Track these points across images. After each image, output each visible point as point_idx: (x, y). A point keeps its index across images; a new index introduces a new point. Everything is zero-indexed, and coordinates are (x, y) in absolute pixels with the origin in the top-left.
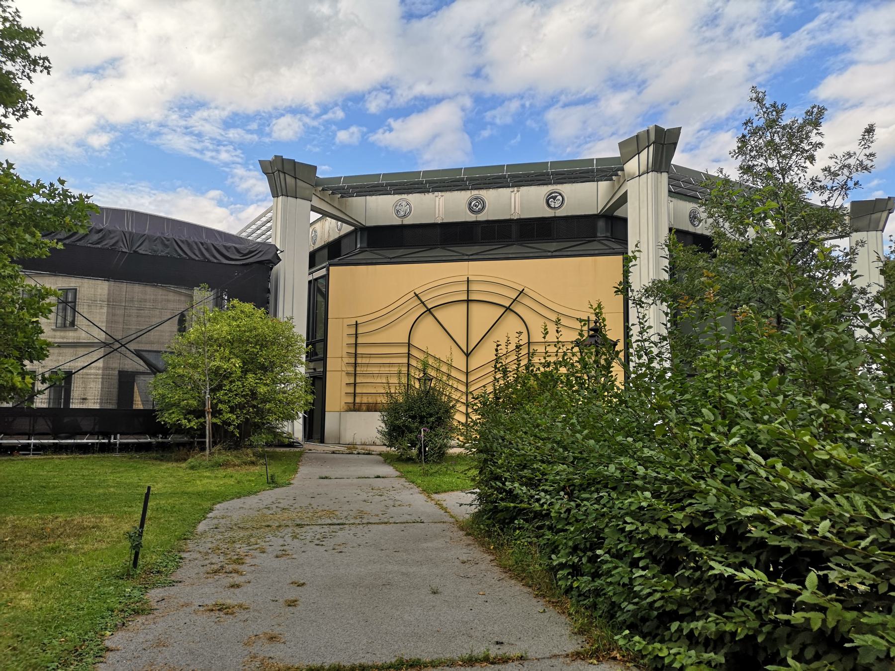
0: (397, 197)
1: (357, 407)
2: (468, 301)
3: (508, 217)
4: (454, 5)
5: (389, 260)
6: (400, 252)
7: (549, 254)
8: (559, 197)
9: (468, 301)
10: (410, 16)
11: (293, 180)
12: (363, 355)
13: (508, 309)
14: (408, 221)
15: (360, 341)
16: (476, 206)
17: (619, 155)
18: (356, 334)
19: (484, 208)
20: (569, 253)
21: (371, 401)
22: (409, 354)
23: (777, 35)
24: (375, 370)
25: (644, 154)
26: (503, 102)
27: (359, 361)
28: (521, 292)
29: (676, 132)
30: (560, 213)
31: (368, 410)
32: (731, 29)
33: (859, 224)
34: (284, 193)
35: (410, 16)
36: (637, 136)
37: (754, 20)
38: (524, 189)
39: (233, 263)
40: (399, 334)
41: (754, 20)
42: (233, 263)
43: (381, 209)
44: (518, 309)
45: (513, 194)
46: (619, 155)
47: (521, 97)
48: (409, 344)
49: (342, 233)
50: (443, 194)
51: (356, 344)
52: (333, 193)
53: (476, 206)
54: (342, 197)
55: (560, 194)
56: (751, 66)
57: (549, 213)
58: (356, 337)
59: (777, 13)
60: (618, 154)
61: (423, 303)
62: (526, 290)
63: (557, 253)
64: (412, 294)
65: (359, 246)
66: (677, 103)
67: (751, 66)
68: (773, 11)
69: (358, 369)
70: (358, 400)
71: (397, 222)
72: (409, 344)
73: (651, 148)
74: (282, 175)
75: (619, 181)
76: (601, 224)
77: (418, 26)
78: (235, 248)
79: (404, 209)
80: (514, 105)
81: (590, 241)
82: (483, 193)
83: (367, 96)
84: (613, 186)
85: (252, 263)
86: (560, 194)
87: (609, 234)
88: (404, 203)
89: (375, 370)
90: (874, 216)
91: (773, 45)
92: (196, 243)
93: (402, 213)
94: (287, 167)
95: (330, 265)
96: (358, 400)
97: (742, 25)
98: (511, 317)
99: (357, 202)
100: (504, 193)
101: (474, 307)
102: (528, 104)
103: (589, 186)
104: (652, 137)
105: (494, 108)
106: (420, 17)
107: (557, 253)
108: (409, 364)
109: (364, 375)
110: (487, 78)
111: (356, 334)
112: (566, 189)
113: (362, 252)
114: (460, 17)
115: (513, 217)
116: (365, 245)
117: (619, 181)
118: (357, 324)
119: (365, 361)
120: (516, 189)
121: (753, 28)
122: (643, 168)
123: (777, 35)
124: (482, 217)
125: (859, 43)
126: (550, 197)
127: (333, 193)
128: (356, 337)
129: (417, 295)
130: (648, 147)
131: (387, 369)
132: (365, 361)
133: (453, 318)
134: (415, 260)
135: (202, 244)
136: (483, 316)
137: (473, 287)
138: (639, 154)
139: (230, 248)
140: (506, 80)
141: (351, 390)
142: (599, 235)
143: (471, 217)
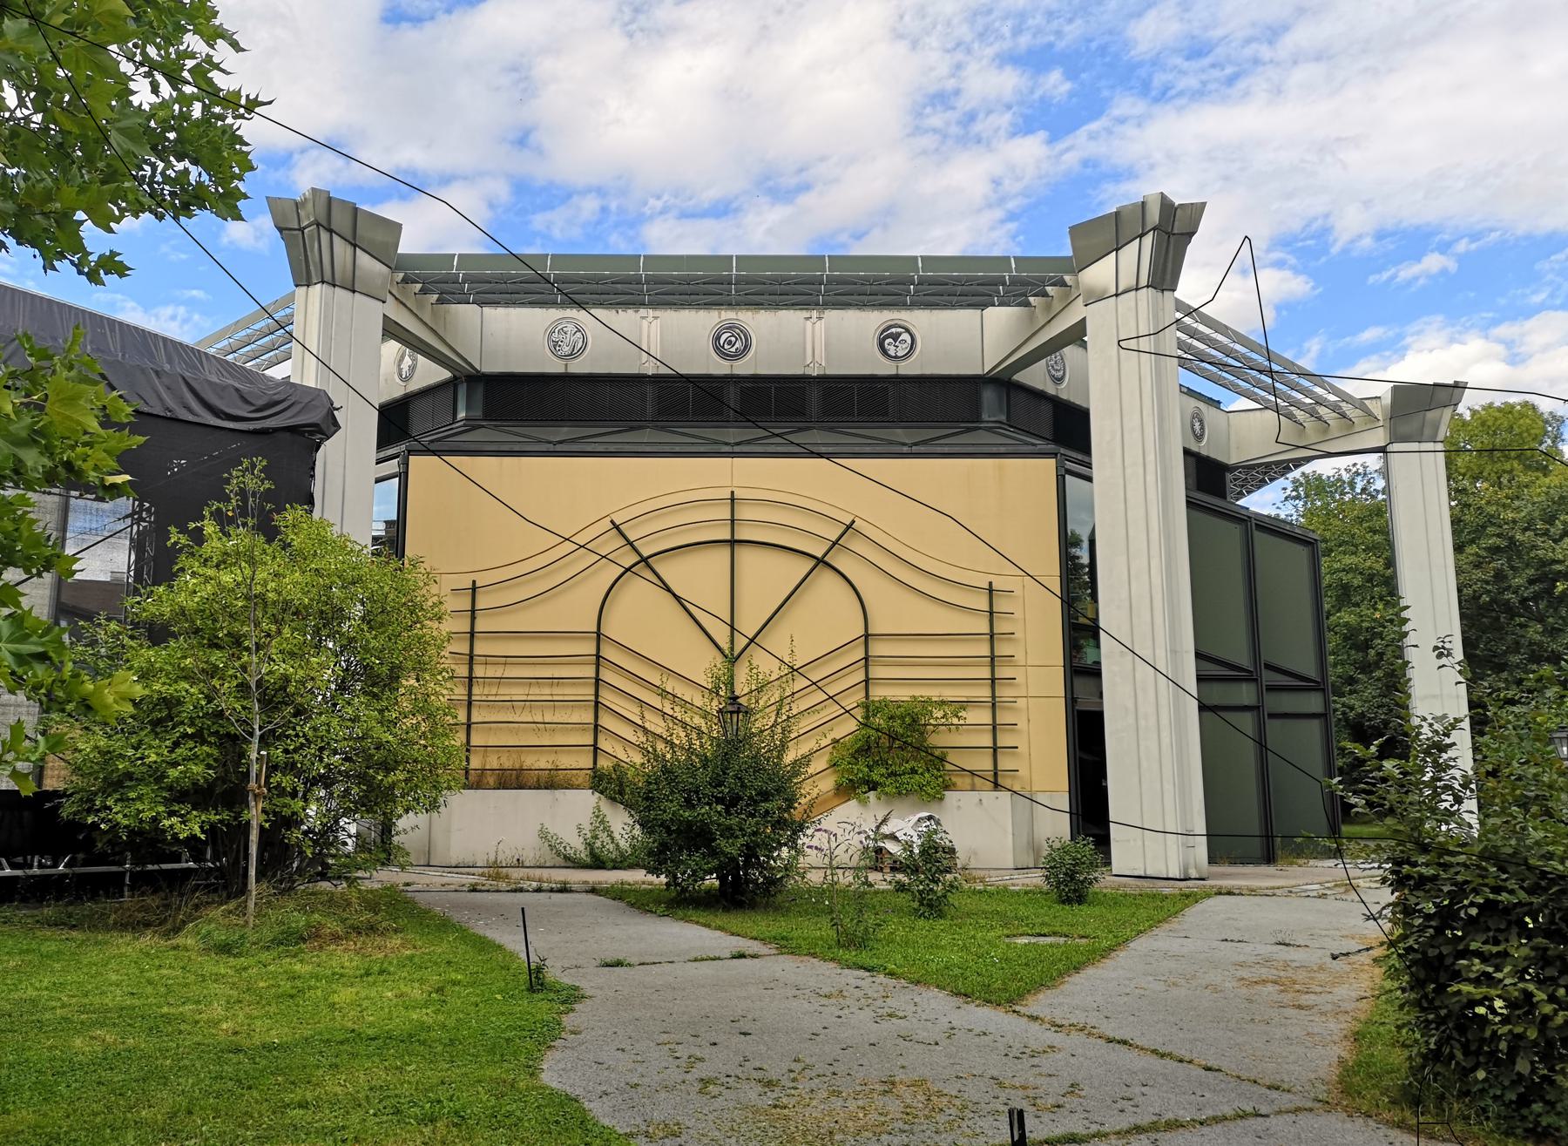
0: (554, 314)
1: (473, 776)
2: (733, 543)
3: (799, 371)
4: (482, 6)
5: (551, 447)
6: (564, 432)
7: (905, 449)
8: (905, 336)
9: (733, 543)
10: (394, 17)
11: (349, 249)
12: (489, 659)
13: (821, 562)
14: (578, 367)
15: (480, 626)
16: (731, 343)
17: (1070, 253)
18: (473, 611)
19: (747, 347)
20: (946, 450)
21: (507, 764)
22: (598, 656)
23: (1042, 135)
24: (518, 693)
25: (1129, 252)
26: (569, 196)
27: (479, 671)
28: (849, 527)
29: (1197, 210)
30: (908, 368)
31: (503, 785)
32: (971, 117)
33: (1404, 429)
34: (328, 276)
35: (394, 17)
36: (1117, 214)
37: (1009, 107)
38: (832, 315)
39: (231, 425)
40: (577, 610)
41: (1009, 107)
42: (231, 425)
43: (516, 338)
44: (841, 561)
45: (809, 323)
46: (1070, 253)
47: (600, 191)
48: (599, 634)
49: (415, 385)
50: (658, 313)
51: (472, 634)
52: (424, 291)
53: (731, 343)
54: (440, 301)
55: (907, 331)
56: (996, 182)
57: (885, 368)
58: (473, 618)
59: (1042, 99)
60: (1068, 251)
61: (631, 544)
62: (858, 524)
63: (922, 449)
64: (606, 524)
65: (462, 415)
66: (866, 233)
67: (996, 182)
68: (1038, 94)
69: (476, 690)
70: (475, 763)
71: (555, 366)
72: (599, 634)
73: (1148, 240)
74: (324, 236)
75: (1048, 307)
76: (988, 395)
77: (409, 36)
78: (237, 390)
79: (569, 340)
80: (590, 205)
81: (969, 430)
82: (749, 319)
83: (296, 157)
84: (1032, 317)
85: (276, 430)
86: (907, 331)
87: (1003, 418)
88: (570, 328)
89: (518, 693)
90: (1430, 415)
91: (1029, 151)
92: (143, 371)
93: (567, 350)
94: (340, 221)
95: (410, 452)
96: (475, 763)
97: (989, 112)
98: (826, 583)
99: (466, 314)
100: (791, 319)
101: (745, 556)
102: (613, 206)
103: (964, 318)
104: (1154, 216)
105: (548, 207)
106: (417, 20)
107: (922, 449)
108: (597, 680)
109: (489, 703)
110: (539, 151)
111: (473, 611)
112: (921, 321)
113: (474, 428)
114: (495, 27)
115: (809, 372)
116: (478, 413)
117: (1048, 307)
118: (474, 589)
119: (491, 672)
120: (815, 314)
121: (1007, 117)
122: (1127, 280)
123: (1042, 135)
124: (743, 367)
125: (1152, 167)
126: (886, 336)
127: (424, 291)
128: (473, 618)
129: (617, 527)
130: (1141, 236)
131: (547, 691)
132: (491, 672)
133: (700, 577)
134: (612, 448)
135: (157, 373)
136: (766, 578)
137: (743, 513)
138: (1117, 250)
139: (224, 388)
140: (570, 160)
141: (1002, 649)
142: (985, 417)
143: (721, 367)
